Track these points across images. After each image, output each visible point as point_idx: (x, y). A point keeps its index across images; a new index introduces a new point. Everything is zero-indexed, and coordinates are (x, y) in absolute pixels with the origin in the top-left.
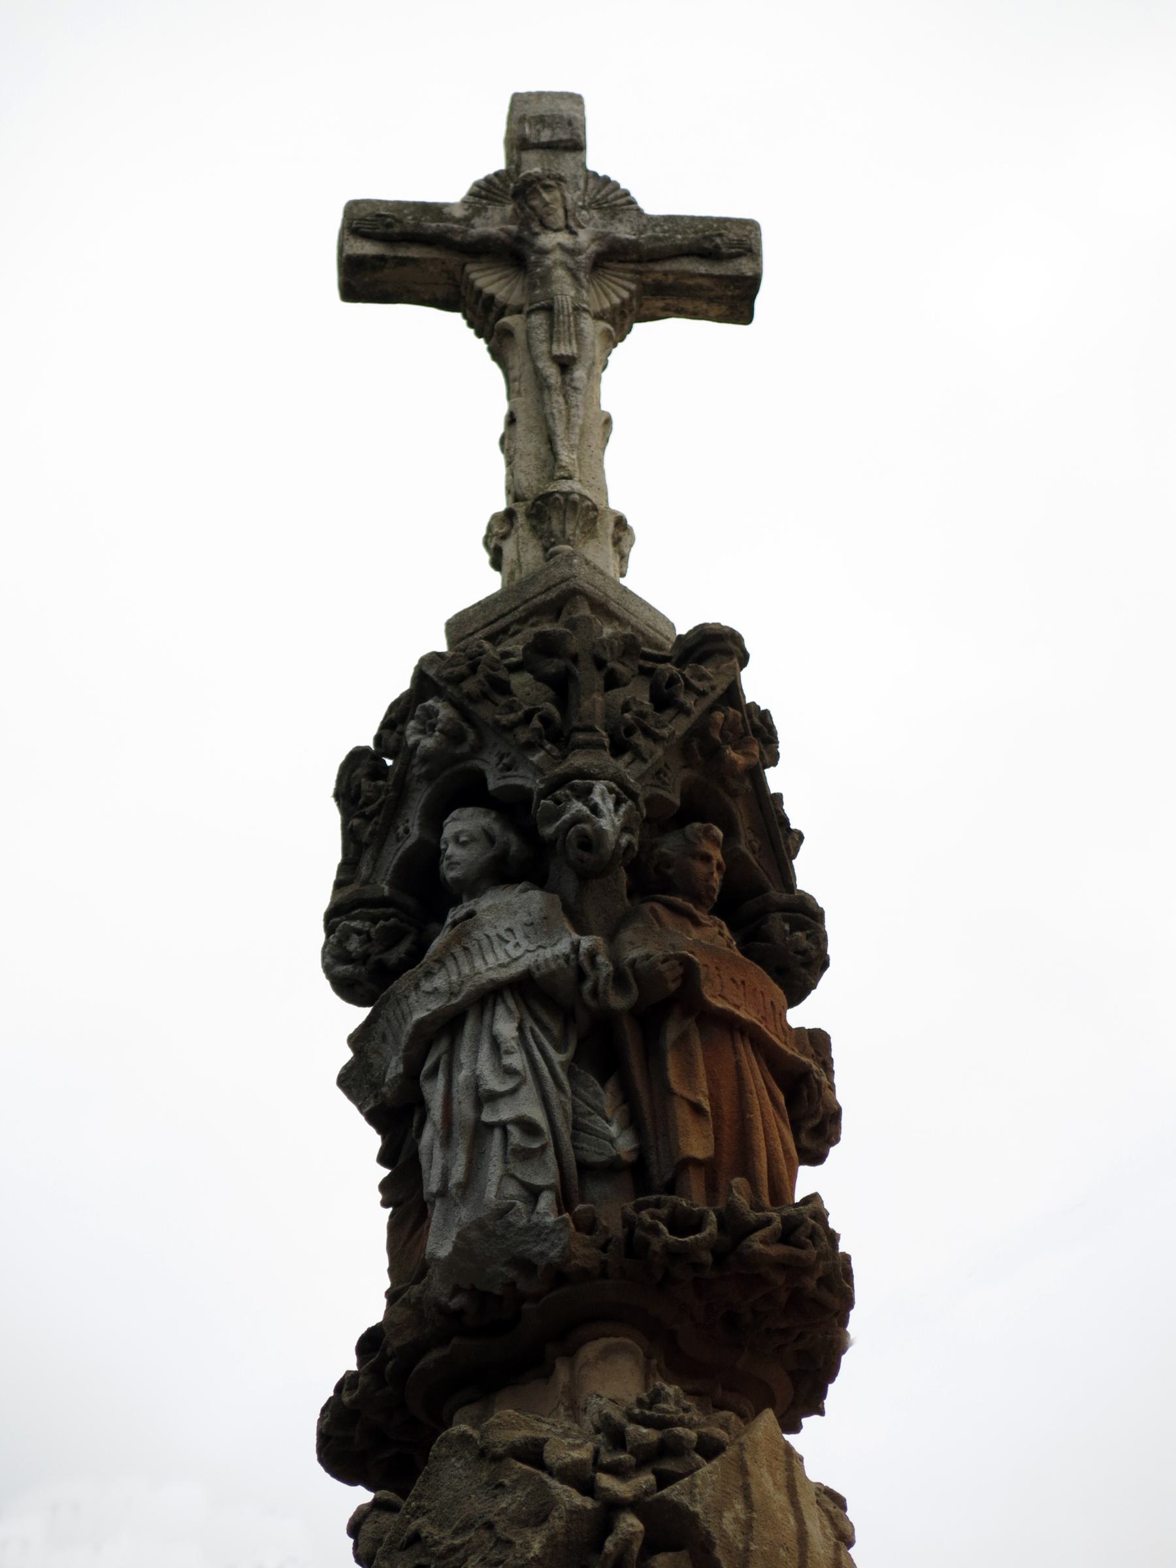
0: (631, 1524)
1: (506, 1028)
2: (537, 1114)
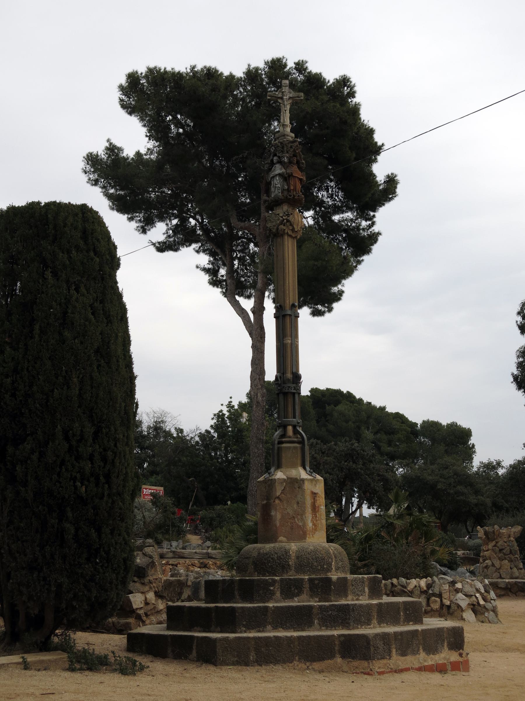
0: (285, 221)
1: (278, 178)
2: (280, 186)
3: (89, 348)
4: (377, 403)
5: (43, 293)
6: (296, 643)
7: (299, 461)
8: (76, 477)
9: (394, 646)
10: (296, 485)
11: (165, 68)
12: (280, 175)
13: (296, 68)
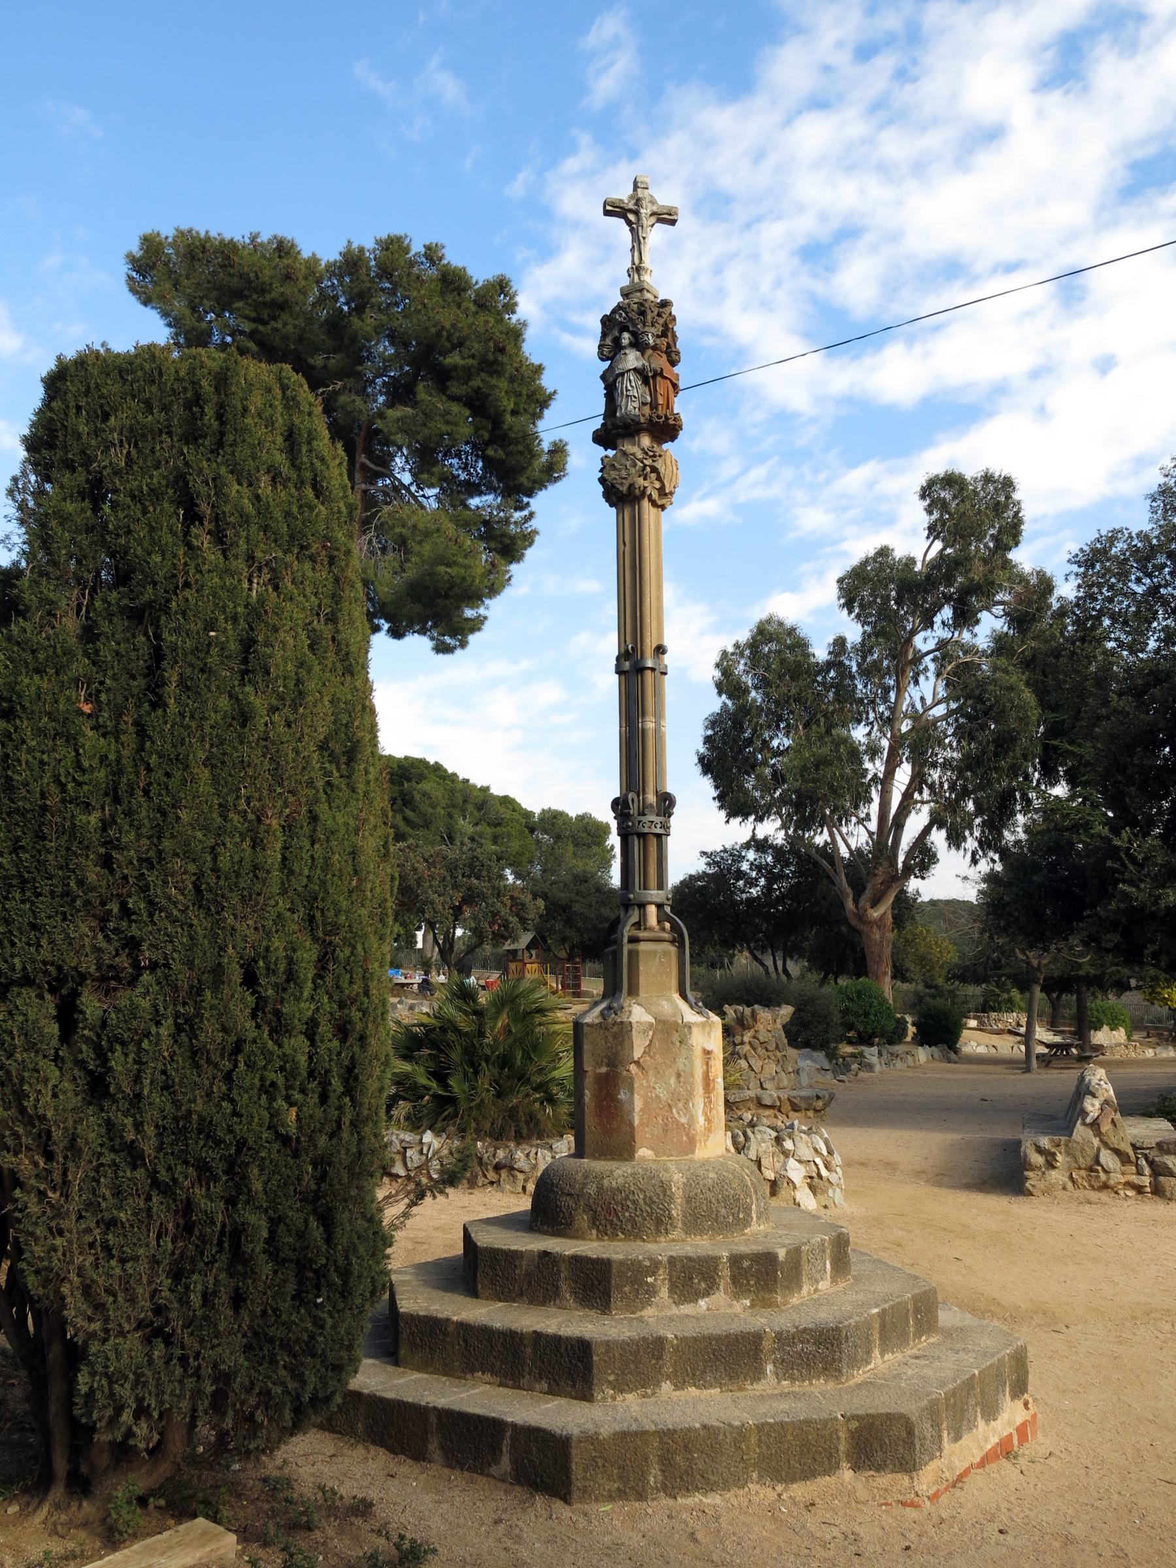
0: (648, 469)
3: (306, 738)
4: (478, 780)
5: (187, 585)
6: (754, 1440)
7: (674, 982)
8: (273, 1084)
9: (945, 1425)
10: (676, 1037)
11: (207, 232)
12: (635, 370)
13: (426, 256)
